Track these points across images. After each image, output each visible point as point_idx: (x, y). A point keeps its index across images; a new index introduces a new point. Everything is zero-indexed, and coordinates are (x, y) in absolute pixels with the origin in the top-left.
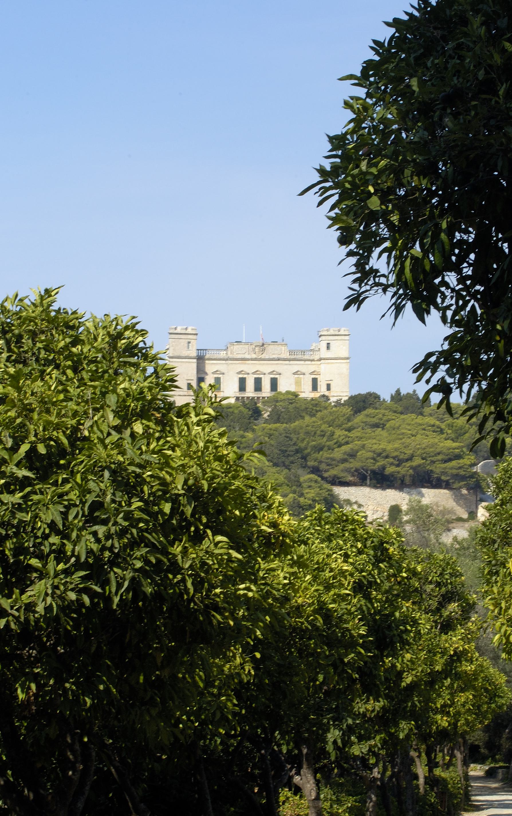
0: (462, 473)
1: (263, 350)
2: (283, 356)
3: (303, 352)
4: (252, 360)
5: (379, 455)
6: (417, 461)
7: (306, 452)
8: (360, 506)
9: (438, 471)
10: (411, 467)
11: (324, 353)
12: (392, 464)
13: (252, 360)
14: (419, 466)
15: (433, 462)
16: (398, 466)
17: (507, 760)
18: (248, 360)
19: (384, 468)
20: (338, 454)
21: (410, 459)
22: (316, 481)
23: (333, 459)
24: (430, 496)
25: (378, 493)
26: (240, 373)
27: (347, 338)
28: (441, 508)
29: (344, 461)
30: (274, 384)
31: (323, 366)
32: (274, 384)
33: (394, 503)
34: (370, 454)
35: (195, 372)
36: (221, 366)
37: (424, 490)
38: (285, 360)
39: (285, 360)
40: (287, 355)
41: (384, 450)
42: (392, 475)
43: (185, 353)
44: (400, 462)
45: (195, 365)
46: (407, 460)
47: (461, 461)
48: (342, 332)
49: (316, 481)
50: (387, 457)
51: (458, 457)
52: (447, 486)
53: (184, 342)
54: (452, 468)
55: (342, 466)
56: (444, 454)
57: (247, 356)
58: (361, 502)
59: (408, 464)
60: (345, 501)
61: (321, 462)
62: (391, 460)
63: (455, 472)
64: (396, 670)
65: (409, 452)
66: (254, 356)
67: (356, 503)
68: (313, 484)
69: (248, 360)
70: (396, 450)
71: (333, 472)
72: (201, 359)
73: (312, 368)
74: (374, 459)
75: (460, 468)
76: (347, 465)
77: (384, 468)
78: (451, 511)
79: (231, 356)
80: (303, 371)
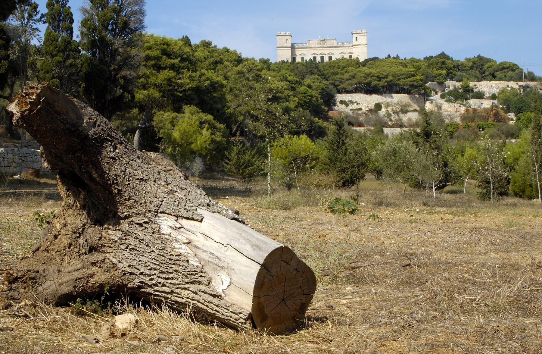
0: (415, 84)
1: (325, 43)
2: (334, 45)
3: (345, 43)
4: (319, 47)
5: (368, 75)
6: (390, 78)
7: (328, 76)
8: (358, 104)
9: (402, 84)
10: (386, 82)
11: (355, 43)
12: (375, 80)
13: (319, 47)
14: (391, 81)
15: (399, 79)
16: (380, 81)
17: (80, 352)
18: (317, 48)
19: (371, 82)
20: (346, 76)
21: (387, 77)
22: (318, 79)
23: (343, 79)
24: (397, 98)
25: (367, 97)
26: (313, 54)
27: (366, 34)
28: (404, 103)
29: (348, 80)
30: (330, 58)
31: (354, 49)
32: (330, 58)
33: (377, 102)
34: (363, 75)
35: (291, 54)
36: (303, 51)
37: (394, 95)
38: (335, 47)
39: (335, 47)
40: (337, 45)
41: (371, 73)
42: (375, 86)
43: (285, 45)
44: (380, 79)
45: (290, 51)
46: (384, 78)
47: (415, 78)
48: (363, 32)
49: (318, 79)
50: (373, 76)
51: (413, 76)
52: (408, 92)
53: (284, 40)
54: (410, 82)
55: (347, 82)
56: (406, 74)
57: (316, 46)
58: (358, 101)
59: (385, 79)
60: (349, 101)
61: (336, 81)
62: (375, 78)
63: (411, 83)
64: (7, 105)
65: (385, 74)
66: (320, 46)
67: (356, 102)
68: (316, 81)
69: (317, 48)
70: (378, 72)
71: (342, 86)
72: (293, 48)
73: (349, 51)
74: (365, 77)
75: (414, 81)
76: (350, 82)
77: (371, 82)
78: (409, 105)
79: (308, 46)
80: (345, 52)
